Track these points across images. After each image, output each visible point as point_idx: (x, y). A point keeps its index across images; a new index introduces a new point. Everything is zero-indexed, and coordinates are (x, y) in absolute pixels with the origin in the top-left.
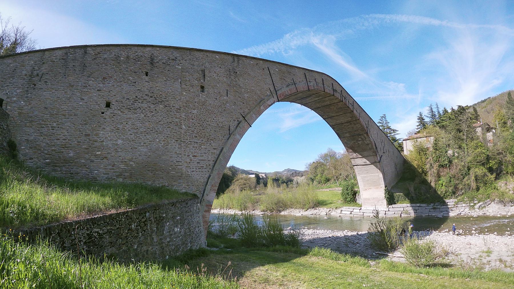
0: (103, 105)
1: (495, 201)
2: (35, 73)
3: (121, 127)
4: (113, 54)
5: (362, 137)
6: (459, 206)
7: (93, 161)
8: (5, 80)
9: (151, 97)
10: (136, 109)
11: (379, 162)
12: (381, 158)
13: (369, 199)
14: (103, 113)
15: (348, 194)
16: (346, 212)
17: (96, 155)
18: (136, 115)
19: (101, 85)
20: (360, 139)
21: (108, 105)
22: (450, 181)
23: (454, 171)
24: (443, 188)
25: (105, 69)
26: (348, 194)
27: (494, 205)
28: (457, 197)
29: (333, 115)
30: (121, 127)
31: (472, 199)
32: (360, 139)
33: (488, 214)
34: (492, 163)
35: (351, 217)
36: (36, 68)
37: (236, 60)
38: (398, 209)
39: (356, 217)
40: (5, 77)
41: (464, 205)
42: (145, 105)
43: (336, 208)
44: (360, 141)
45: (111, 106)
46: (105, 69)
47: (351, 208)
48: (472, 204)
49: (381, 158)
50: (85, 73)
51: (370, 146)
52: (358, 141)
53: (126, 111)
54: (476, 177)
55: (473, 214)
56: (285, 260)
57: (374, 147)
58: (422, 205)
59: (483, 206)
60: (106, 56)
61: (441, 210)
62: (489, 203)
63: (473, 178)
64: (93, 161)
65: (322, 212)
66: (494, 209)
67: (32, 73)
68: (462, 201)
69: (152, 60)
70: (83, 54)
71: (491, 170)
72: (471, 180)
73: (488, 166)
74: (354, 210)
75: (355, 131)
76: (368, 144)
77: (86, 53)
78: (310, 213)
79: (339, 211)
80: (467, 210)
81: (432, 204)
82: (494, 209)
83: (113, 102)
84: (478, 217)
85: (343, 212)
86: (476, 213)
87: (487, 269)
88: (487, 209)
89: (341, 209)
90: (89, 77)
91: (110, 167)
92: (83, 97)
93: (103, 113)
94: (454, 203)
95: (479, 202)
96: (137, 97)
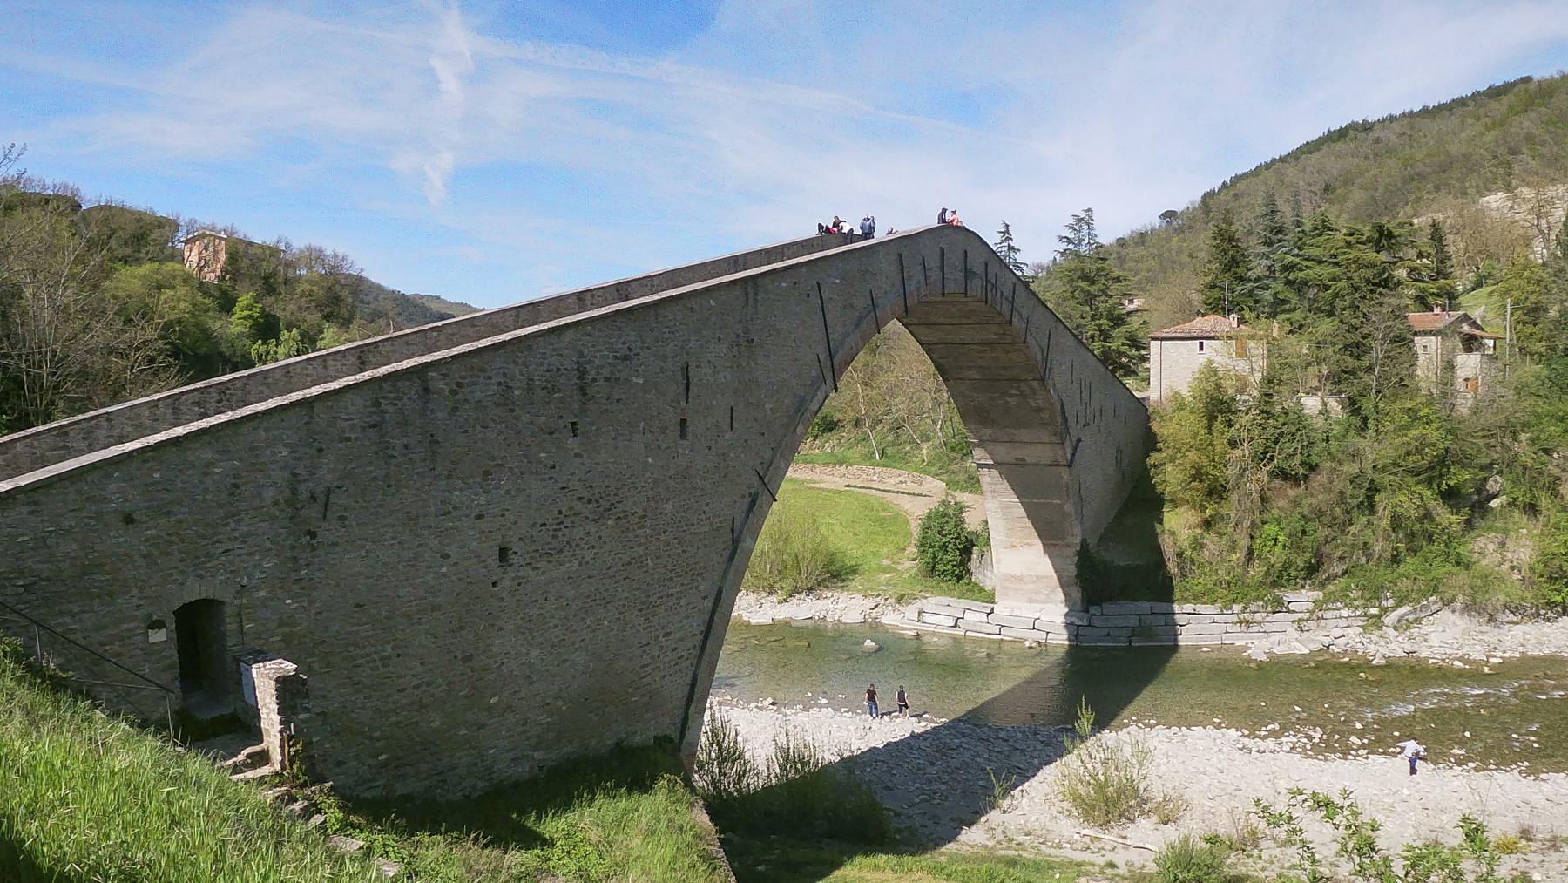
0: (493, 560)
1: (1458, 605)
3: (535, 612)
5: (1024, 387)
6: (1328, 614)
7: (482, 726)
9: (590, 501)
10: (561, 551)
11: (1069, 466)
12: (1075, 448)
13: (1021, 579)
14: (494, 584)
15: (944, 547)
16: (937, 616)
17: (489, 709)
18: (563, 569)
19: (483, 499)
21: (503, 553)
22: (1304, 533)
23: (1317, 494)
24: (1278, 549)
25: (483, 441)
26: (944, 547)
27: (1452, 617)
28: (1322, 584)
29: (942, 320)
30: (535, 612)
31: (1374, 593)
33: (1424, 653)
34: (1460, 476)
35: (955, 639)
37: (751, 291)
38: (1120, 621)
39: (975, 640)
41: (1345, 613)
42: (578, 533)
43: (900, 599)
44: (1011, 396)
45: (513, 558)
46: (483, 441)
47: (956, 605)
48: (1374, 611)
49: (1075, 448)
50: (439, 470)
51: (1045, 415)
53: (543, 565)
54: (1396, 521)
55: (1372, 649)
57: (1059, 419)
58: (1201, 608)
59: (1411, 617)
61: (1266, 627)
62: (1434, 608)
63: (1385, 523)
64: (482, 726)
65: (843, 608)
66: (1446, 636)
68: (1343, 598)
69: (582, 373)
71: (1451, 496)
72: (1375, 531)
73: (1444, 487)
74: (968, 615)
75: (1004, 368)
76: (1039, 410)
77: (427, 390)
78: (801, 610)
79: (910, 612)
80: (1354, 632)
81: (1237, 608)
82: (1446, 636)
84: (1390, 665)
85: (927, 618)
86: (1387, 645)
88: (1425, 629)
89: (918, 605)
90: (449, 477)
91: (520, 729)
92: (447, 550)
93: (494, 584)
94: (1310, 606)
95: (1397, 606)
96: (560, 512)
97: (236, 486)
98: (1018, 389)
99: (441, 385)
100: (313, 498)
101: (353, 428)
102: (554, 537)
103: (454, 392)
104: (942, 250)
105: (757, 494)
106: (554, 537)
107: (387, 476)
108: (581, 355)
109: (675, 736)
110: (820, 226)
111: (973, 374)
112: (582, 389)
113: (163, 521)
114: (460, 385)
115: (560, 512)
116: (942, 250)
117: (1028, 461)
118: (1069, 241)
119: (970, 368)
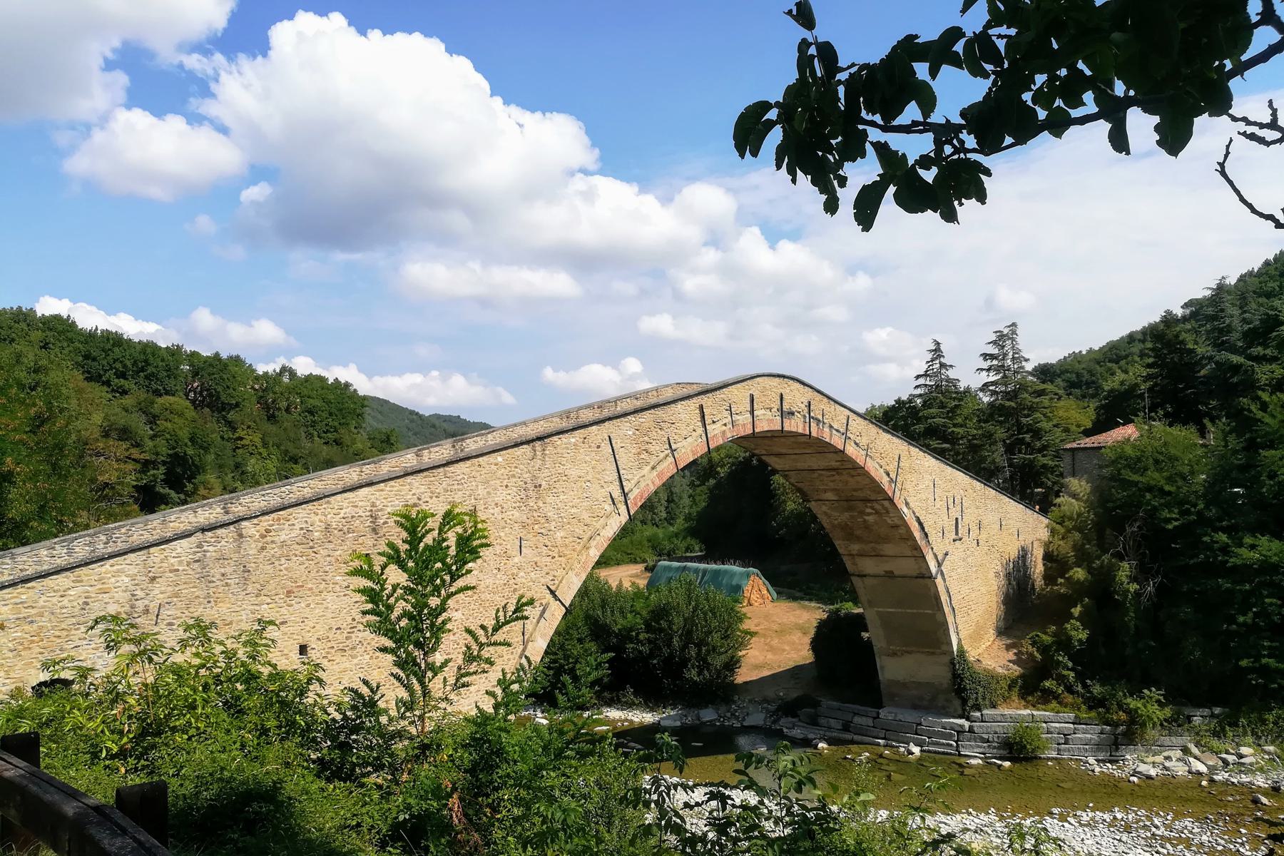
2: (140, 605)
4: (297, 527)
5: (877, 506)
8: (65, 633)
10: (353, 648)
18: (355, 661)
20: (869, 510)
25: (286, 569)
32: (869, 510)
36: (140, 593)
40: (63, 626)
44: (869, 514)
46: (286, 569)
50: (250, 589)
52: (862, 513)
53: (338, 658)
56: (795, 599)
60: (283, 537)
67: (132, 607)
69: (374, 518)
70: (235, 540)
77: (241, 536)
83: (313, 644)
87: (390, 777)
96: (354, 620)
97: (87, 604)
98: (872, 508)
99: (252, 531)
100: (147, 611)
101: (180, 563)
102: (347, 638)
103: (263, 536)
104: (752, 397)
105: (547, 604)
106: (347, 638)
107: (208, 596)
108: (373, 505)
109: (210, 108)
110: (982, 198)
111: (830, 496)
112: (374, 530)
113: (27, 627)
114: (268, 531)
115: (354, 620)
116: (752, 397)
117: (896, 573)
118: (992, 357)
119: (825, 491)
